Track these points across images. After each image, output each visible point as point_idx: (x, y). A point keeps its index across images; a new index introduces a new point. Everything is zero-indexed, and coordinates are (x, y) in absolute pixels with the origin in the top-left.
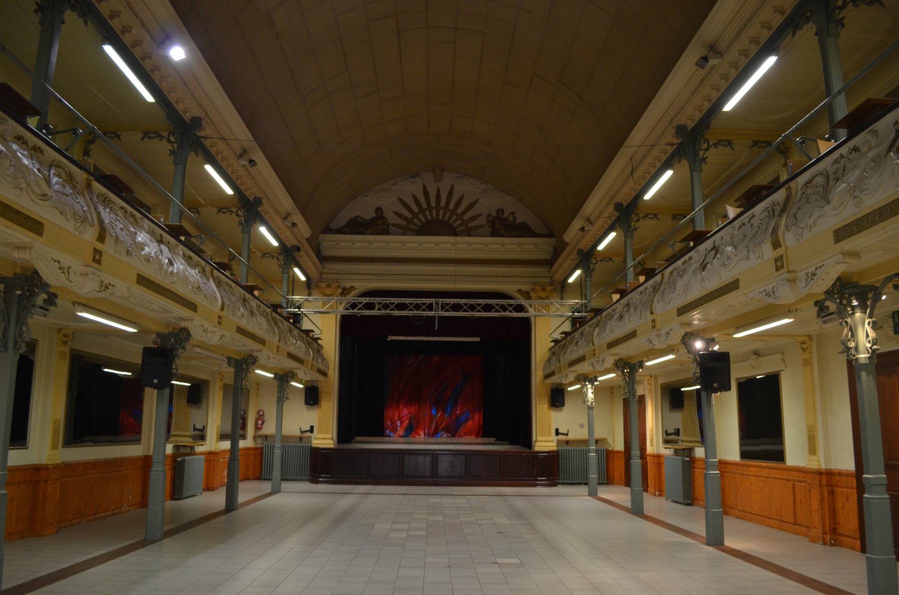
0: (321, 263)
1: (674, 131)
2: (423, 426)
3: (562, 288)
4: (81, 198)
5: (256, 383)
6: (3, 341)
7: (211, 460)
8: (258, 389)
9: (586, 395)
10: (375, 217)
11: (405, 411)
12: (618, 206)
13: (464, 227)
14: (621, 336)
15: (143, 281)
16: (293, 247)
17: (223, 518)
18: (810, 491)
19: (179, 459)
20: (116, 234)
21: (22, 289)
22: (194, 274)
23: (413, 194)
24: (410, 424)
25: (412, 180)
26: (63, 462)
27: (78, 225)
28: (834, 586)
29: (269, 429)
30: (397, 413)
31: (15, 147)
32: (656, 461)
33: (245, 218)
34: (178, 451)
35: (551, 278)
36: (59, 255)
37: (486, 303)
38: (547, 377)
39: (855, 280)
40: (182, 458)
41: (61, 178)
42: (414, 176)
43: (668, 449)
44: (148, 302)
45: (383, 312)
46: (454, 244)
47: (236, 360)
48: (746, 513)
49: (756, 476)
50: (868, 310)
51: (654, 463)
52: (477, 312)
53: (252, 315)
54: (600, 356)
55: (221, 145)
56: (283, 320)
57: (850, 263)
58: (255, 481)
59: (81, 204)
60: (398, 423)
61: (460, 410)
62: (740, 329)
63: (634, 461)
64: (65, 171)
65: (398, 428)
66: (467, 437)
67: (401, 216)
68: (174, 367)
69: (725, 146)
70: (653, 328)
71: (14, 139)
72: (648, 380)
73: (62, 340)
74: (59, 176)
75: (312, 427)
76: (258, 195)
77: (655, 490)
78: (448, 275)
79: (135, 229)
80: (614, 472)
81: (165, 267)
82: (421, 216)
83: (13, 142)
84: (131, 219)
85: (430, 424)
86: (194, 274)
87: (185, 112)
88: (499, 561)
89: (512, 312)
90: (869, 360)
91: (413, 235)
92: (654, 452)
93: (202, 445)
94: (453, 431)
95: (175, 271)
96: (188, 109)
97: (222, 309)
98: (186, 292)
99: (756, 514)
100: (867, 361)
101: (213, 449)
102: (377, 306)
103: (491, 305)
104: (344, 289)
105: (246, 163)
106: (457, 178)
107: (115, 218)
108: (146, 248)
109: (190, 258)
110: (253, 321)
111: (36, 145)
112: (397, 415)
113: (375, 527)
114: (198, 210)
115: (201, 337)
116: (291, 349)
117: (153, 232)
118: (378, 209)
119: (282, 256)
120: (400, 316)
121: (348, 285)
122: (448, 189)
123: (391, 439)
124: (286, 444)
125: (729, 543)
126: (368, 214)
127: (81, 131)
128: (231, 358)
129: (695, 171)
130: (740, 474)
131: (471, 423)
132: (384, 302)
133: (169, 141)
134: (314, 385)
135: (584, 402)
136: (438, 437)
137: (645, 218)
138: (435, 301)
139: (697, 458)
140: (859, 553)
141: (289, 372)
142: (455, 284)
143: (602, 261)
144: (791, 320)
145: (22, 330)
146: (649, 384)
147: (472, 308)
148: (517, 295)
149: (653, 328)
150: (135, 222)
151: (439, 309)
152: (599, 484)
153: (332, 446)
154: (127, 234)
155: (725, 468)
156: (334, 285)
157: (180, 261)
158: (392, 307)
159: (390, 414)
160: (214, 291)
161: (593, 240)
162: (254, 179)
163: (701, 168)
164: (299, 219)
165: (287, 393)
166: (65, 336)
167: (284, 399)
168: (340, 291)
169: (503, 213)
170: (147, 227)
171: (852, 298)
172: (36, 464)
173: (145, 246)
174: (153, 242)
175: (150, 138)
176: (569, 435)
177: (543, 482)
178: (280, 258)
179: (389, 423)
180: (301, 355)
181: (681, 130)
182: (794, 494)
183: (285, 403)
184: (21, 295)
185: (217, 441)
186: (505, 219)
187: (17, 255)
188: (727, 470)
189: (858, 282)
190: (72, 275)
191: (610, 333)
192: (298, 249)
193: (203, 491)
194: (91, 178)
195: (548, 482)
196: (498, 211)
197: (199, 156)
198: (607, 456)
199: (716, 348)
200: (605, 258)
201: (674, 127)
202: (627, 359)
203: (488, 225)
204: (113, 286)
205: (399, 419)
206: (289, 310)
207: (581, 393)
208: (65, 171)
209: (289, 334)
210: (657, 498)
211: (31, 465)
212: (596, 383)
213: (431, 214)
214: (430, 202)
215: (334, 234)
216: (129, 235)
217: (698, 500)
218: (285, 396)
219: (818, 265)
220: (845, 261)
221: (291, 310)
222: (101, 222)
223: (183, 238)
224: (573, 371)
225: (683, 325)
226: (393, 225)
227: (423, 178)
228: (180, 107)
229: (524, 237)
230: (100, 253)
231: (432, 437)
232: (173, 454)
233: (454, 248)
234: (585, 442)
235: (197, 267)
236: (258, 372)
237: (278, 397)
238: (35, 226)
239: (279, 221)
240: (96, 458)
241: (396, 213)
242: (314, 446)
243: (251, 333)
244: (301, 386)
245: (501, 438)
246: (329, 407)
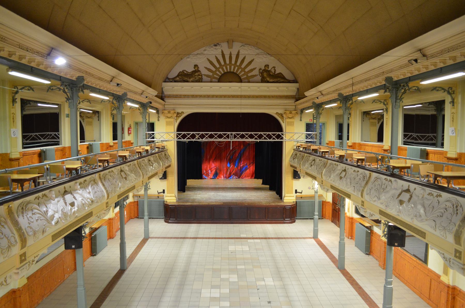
10: (194, 71)
18: (441, 292)
24: (216, 171)
30: (209, 166)
32: (350, 221)
42: (216, 45)
51: (349, 221)
60: (210, 171)
67: (209, 70)
75: (164, 190)
77: (349, 235)
80: (326, 212)
82: (221, 70)
102: (197, 136)
104: (178, 113)
112: (209, 167)
121: (180, 111)
122: (236, 53)
126: (190, 69)
131: (249, 171)
151: (232, 138)
156: (172, 112)
158: (207, 136)
168: (175, 115)
169: (268, 68)
179: (205, 172)
192: (151, 103)
195: (291, 221)
196: (265, 66)
198: (323, 204)
211: (10, 290)
214: (225, 61)
221: (149, 140)
226: (205, 75)
241: (206, 68)
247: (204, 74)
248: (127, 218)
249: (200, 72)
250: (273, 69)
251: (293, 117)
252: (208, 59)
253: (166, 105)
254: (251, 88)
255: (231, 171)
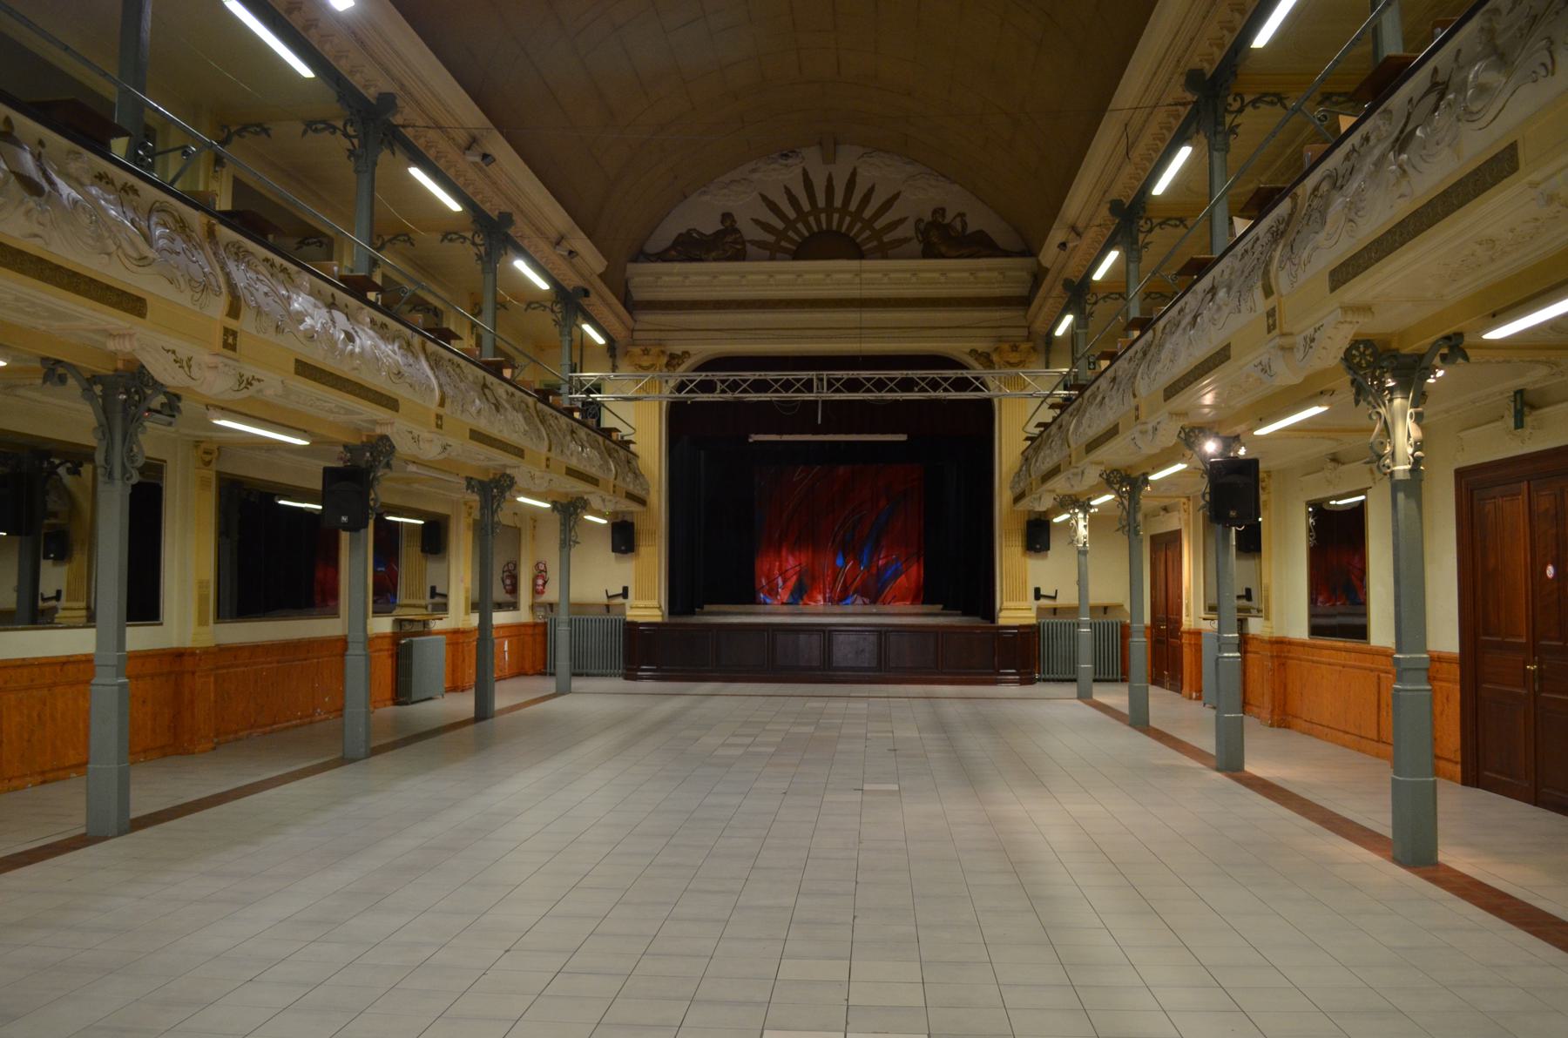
0: (630, 313)
1: (1183, 80)
2: (822, 586)
3: (1047, 346)
4: (199, 254)
5: (532, 519)
6: (106, 468)
7: (457, 643)
8: (534, 527)
9: (1075, 531)
11: (791, 561)
12: (1116, 207)
13: (875, 243)
14: (1101, 433)
15: (305, 369)
16: (576, 289)
17: (471, 728)
19: (403, 642)
20: (256, 303)
21: (127, 392)
22: (390, 352)
23: (786, 188)
24: (799, 580)
25: (785, 162)
26: (217, 645)
27: (197, 296)
28: (1350, 818)
29: (552, 594)
30: (777, 564)
31: (94, 191)
32: (1193, 642)
33: (486, 248)
34: (401, 629)
35: (1029, 327)
36: (172, 343)
37: (904, 376)
38: (1018, 498)
39: (1394, 345)
40: (408, 639)
41: (167, 228)
43: (1209, 621)
44: (318, 399)
45: (729, 396)
46: (858, 273)
47: (481, 482)
48: (1315, 726)
49: (1330, 664)
50: (1411, 395)
52: (888, 391)
53: (497, 410)
54: (1078, 465)
55: (432, 134)
56: (558, 415)
57: (1358, 322)
58: (536, 677)
59: (202, 262)
61: (884, 558)
62: (1263, 421)
63: (1136, 639)
64: (173, 216)
65: (780, 590)
66: (897, 603)
67: (767, 227)
68: (373, 496)
69: (1272, 103)
70: (1136, 420)
71: (94, 179)
72: (1184, 504)
73: (203, 461)
74: (165, 225)
75: (625, 589)
76: (504, 208)
77: (1190, 690)
78: (851, 328)
79: (288, 291)
81: (340, 345)
82: (800, 226)
83: (92, 185)
84: (281, 276)
85: (835, 580)
86: (390, 352)
87: (366, 87)
88: (866, 787)
89: (949, 391)
90: (1411, 475)
91: (789, 260)
92: (1190, 625)
93: (441, 619)
94: (874, 593)
95: (357, 350)
96: (371, 82)
97: (442, 404)
98: (380, 382)
99: (1328, 727)
100: (1408, 476)
101: (460, 626)
103: (912, 379)
104: (672, 356)
105: (478, 159)
106: (862, 156)
107: (255, 279)
108: (306, 319)
109: (384, 326)
110: (500, 420)
111: (126, 184)
112: (777, 568)
113: (699, 741)
114: (409, 239)
115: (409, 449)
116: (574, 463)
117: (319, 292)
118: (726, 216)
119: (559, 306)
120: (758, 401)
121: (678, 349)
122: (847, 176)
123: (767, 608)
124: (583, 617)
125: (1252, 767)
126: (710, 226)
127: (194, 149)
128: (471, 478)
129: (1216, 150)
130: (1308, 661)
131: (905, 580)
132: (732, 378)
133: (346, 135)
134: (626, 519)
135: (1072, 542)
136: (847, 604)
137: (1163, 226)
138: (817, 375)
139: (1250, 636)
140: (1460, 786)
141: (578, 498)
142: (861, 343)
143: (1107, 299)
144: (1324, 409)
145: (132, 451)
146: (1185, 511)
147: (880, 385)
148: (970, 361)
149: (1136, 420)
150: (290, 282)
152: (1095, 681)
153: (659, 619)
154: (276, 302)
155: (1289, 652)
156: (654, 350)
157: (366, 333)
158: (745, 386)
159: (766, 567)
160: (427, 376)
161: (1081, 268)
162: (495, 183)
163: (1227, 145)
164: (581, 243)
165: (576, 533)
166: (206, 452)
167: (571, 543)
168: (664, 360)
169: (944, 216)
170: (308, 285)
171: (1386, 375)
172: (177, 648)
173: (306, 316)
174: (320, 308)
175: (316, 130)
176: (1058, 597)
177: (1013, 677)
178: (556, 308)
179: (764, 582)
180: (594, 471)
181: (1194, 79)
182: (1379, 692)
183: (572, 550)
184: (126, 400)
185: (467, 613)
186: (949, 225)
187: (112, 345)
188: (1290, 655)
189: (1397, 350)
190: (194, 369)
191: (1089, 426)
192: (586, 293)
193: (447, 692)
194: (214, 221)
195: (1018, 677)
196: (935, 212)
197: (398, 152)
199: (1242, 452)
200: (1112, 294)
201: (1182, 74)
202: (1126, 471)
203: (918, 237)
204: (259, 380)
205: (780, 575)
206: (574, 396)
207: (1068, 527)
208: (173, 216)
209: (569, 438)
210: (1194, 702)
212: (1092, 511)
213: (797, 232)
215: (652, 261)
216: (279, 301)
217: (1251, 705)
218: (573, 538)
219: (1317, 326)
220: (1348, 320)
221: (577, 396)
222: (232, 287)
223: (372, 296)
224: (1050, 491)
225: (1174, 416)
226: (753, 242)
227: (803, 158)
228: (356, 81)
229: (979, 257)
230: (234, 334)
231: (838, 604)
232: (393, 633)
233: (857, 280)
234: (1073, 611)
235: (397, 340)
236: (522, 499)
237: (561, 540)
238: (134, 304)
239: (545, 248)
240: (271, 639)
241: (757, 222)
242: (629, 619)
243: (495, 440)
244: (604, 522)
245: (950, 606)
246: (652, 559)
247: (749, 239)
248: (509, 665)
249: (740, 232)
250: (959, 219)
251: (1021, 362)
252: (762, 195)
253: (639, 330)
254: (892, 275)
255: (849, 582)
